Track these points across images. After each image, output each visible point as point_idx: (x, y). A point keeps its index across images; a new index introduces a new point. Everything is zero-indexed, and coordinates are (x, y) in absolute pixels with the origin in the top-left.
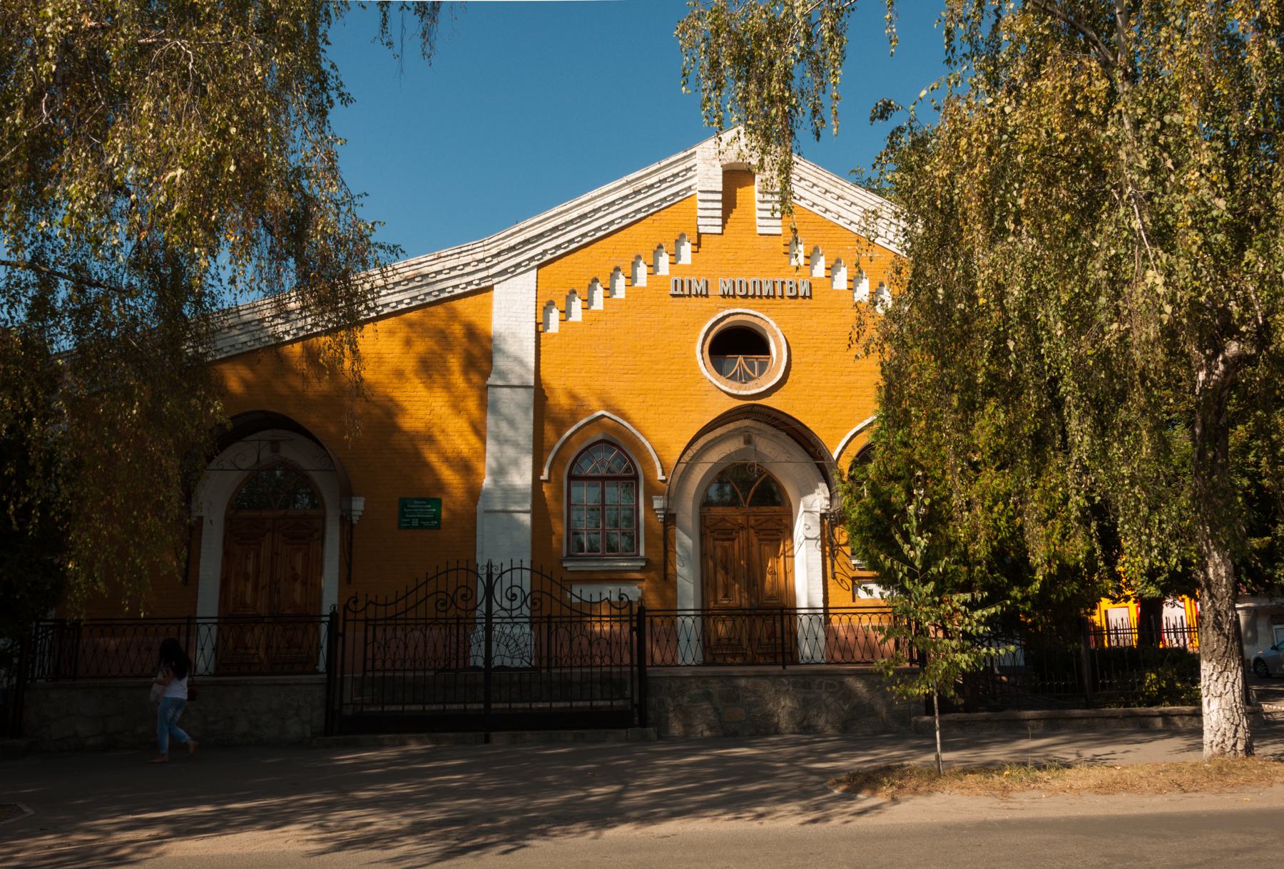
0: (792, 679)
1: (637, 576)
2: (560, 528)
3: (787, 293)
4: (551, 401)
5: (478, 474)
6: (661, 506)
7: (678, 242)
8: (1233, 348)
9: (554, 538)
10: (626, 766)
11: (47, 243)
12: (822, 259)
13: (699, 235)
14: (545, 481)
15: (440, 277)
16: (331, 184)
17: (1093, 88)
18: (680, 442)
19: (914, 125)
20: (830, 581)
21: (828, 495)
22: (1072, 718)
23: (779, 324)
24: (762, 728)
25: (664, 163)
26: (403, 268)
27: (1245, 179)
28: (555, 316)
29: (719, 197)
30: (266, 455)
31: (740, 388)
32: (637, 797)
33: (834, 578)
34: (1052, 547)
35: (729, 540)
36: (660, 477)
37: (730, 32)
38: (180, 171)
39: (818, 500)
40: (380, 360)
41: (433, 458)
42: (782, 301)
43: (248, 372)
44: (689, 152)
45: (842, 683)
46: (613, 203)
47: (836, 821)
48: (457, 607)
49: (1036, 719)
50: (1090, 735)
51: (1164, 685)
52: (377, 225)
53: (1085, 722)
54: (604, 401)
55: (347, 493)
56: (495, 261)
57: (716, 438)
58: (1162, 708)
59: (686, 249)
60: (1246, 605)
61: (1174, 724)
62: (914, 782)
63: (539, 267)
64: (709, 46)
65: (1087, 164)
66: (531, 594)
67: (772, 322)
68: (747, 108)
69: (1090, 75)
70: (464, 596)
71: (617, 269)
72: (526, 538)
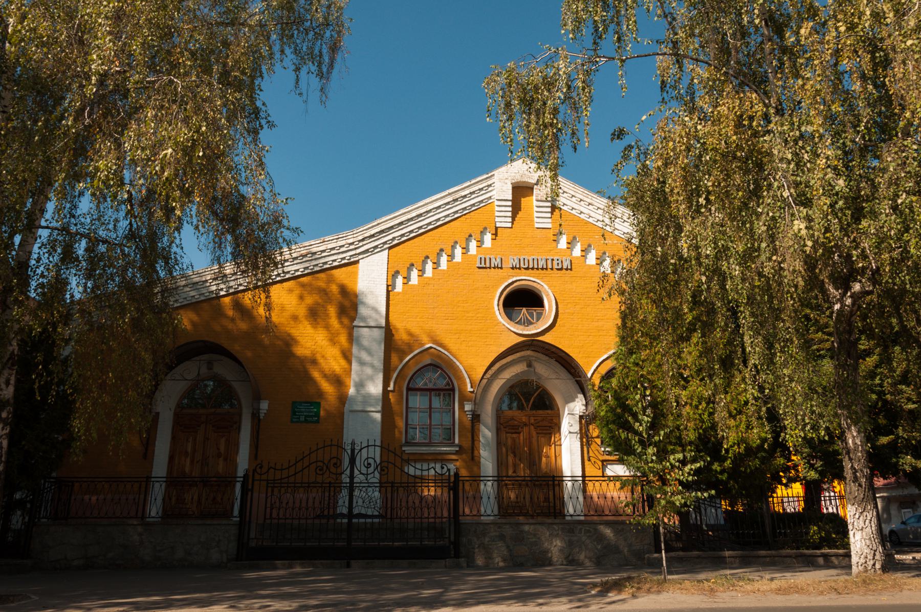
0: (560, 526)
1: (454, 457)
2: (401, 423)
3: (555, 266)
4: (396, 337)
5: (346, 386)
6: (470, 409)
7: (483, 233)
8: (857, 287)
9: (396, 430)
10: (447, 580)
11: (73, 220)
12: (579, 244)
13: (496, 228)
14: (391, 391)
15: (324, 254)
16: (261, 174)
17: (753, 110)
18: (483, 366)
19: (640, 143)
20: (587, 463)
21: (584, 402)
22: (759, 557)
23: (550, 287)
24: (541, 560)
25: (473, 181)
26: (298, 250)
27: (858, 173)
28: (400, 281)
29: (510, 203)
30: (204, 370)
31: (523, 330)
32: (453, 595)
33: (589, 460)
34: (740, 434)
35: (516, 433)
36: (469, 389)
37: (518, 84)
38: (170, 151)
39: (578, 406)
40: (283, 309)
41: (316, 375)
42: (552, 272)
43: (194, 315)
44: (490, 175)
45: (596, 530)
46: (439, 207)
47: (593, 607)
48: (330, 472)
49: (733, 557)
50: (772, 568)
51: (823, 535)
52: (289, 200)
53: (768, 559)
54: (432, 338)
55: (257, 397)
56: (361, 244)
57: (508, 363)
58: (823, 551)
59: (488, 238)
60: (882, 495)
61: (832, 562)
62: (648, 586)
63: (390, 248)
64: (504, 93)
65: (752, 160)
66: (380, 464)
67: (545, 286)
68: (529, 131)
69: (751, 102)
70: (335, 464)
71: (442, 250)
72: (378, 429)
